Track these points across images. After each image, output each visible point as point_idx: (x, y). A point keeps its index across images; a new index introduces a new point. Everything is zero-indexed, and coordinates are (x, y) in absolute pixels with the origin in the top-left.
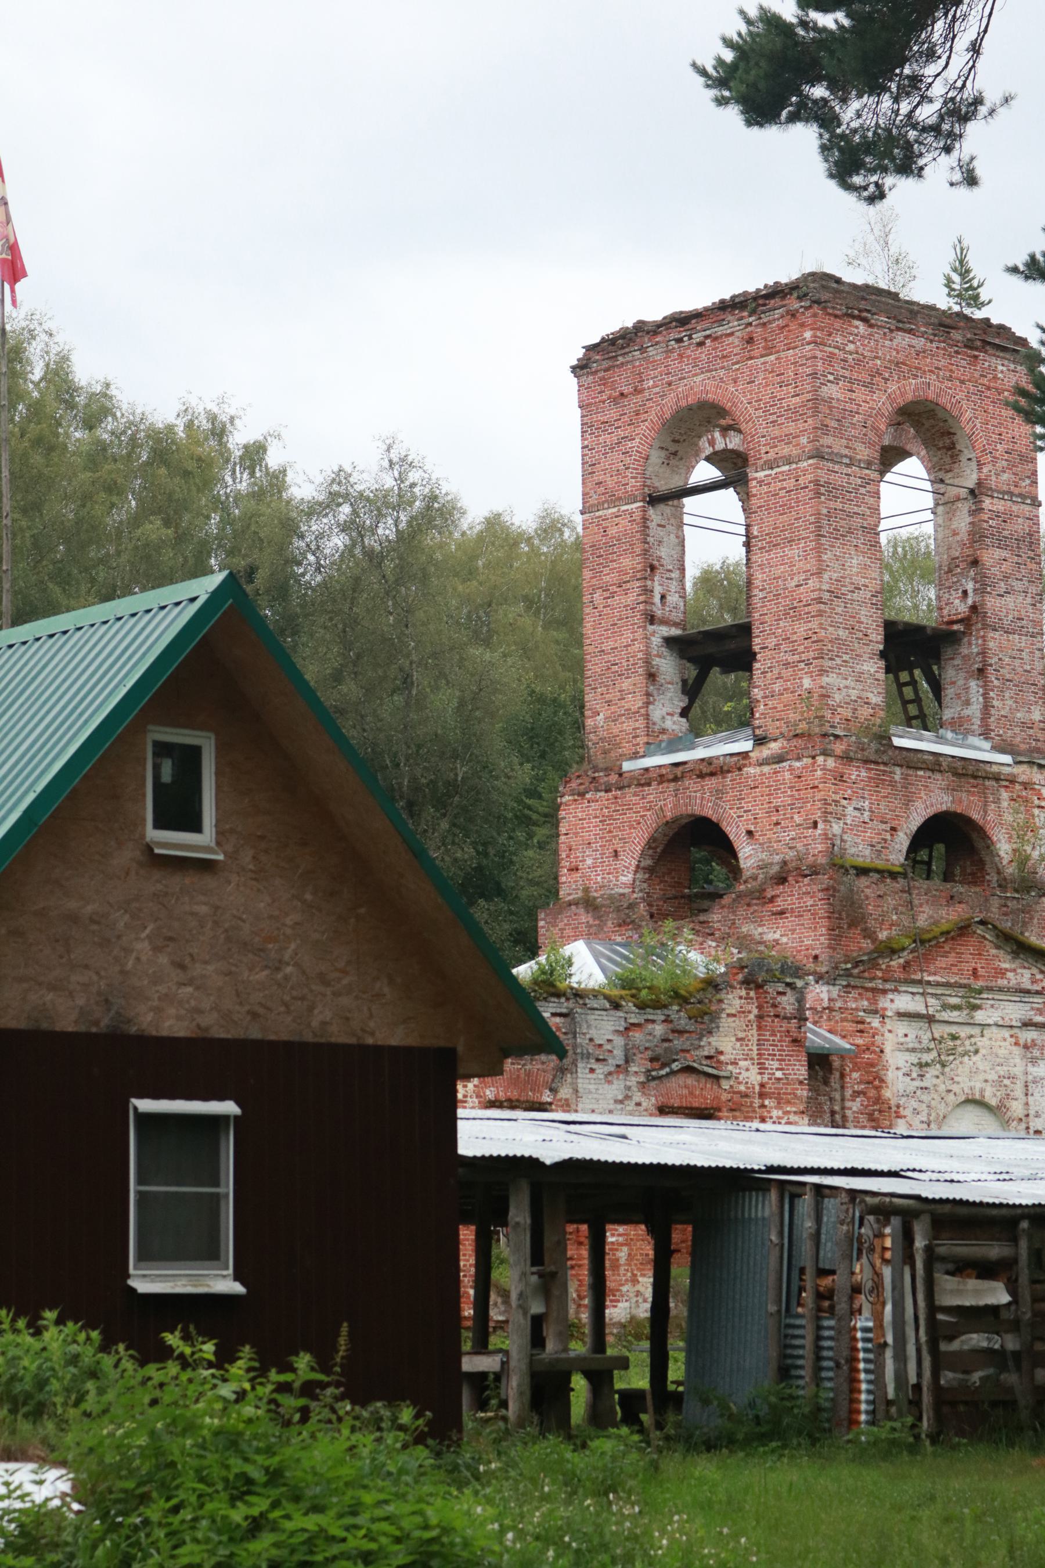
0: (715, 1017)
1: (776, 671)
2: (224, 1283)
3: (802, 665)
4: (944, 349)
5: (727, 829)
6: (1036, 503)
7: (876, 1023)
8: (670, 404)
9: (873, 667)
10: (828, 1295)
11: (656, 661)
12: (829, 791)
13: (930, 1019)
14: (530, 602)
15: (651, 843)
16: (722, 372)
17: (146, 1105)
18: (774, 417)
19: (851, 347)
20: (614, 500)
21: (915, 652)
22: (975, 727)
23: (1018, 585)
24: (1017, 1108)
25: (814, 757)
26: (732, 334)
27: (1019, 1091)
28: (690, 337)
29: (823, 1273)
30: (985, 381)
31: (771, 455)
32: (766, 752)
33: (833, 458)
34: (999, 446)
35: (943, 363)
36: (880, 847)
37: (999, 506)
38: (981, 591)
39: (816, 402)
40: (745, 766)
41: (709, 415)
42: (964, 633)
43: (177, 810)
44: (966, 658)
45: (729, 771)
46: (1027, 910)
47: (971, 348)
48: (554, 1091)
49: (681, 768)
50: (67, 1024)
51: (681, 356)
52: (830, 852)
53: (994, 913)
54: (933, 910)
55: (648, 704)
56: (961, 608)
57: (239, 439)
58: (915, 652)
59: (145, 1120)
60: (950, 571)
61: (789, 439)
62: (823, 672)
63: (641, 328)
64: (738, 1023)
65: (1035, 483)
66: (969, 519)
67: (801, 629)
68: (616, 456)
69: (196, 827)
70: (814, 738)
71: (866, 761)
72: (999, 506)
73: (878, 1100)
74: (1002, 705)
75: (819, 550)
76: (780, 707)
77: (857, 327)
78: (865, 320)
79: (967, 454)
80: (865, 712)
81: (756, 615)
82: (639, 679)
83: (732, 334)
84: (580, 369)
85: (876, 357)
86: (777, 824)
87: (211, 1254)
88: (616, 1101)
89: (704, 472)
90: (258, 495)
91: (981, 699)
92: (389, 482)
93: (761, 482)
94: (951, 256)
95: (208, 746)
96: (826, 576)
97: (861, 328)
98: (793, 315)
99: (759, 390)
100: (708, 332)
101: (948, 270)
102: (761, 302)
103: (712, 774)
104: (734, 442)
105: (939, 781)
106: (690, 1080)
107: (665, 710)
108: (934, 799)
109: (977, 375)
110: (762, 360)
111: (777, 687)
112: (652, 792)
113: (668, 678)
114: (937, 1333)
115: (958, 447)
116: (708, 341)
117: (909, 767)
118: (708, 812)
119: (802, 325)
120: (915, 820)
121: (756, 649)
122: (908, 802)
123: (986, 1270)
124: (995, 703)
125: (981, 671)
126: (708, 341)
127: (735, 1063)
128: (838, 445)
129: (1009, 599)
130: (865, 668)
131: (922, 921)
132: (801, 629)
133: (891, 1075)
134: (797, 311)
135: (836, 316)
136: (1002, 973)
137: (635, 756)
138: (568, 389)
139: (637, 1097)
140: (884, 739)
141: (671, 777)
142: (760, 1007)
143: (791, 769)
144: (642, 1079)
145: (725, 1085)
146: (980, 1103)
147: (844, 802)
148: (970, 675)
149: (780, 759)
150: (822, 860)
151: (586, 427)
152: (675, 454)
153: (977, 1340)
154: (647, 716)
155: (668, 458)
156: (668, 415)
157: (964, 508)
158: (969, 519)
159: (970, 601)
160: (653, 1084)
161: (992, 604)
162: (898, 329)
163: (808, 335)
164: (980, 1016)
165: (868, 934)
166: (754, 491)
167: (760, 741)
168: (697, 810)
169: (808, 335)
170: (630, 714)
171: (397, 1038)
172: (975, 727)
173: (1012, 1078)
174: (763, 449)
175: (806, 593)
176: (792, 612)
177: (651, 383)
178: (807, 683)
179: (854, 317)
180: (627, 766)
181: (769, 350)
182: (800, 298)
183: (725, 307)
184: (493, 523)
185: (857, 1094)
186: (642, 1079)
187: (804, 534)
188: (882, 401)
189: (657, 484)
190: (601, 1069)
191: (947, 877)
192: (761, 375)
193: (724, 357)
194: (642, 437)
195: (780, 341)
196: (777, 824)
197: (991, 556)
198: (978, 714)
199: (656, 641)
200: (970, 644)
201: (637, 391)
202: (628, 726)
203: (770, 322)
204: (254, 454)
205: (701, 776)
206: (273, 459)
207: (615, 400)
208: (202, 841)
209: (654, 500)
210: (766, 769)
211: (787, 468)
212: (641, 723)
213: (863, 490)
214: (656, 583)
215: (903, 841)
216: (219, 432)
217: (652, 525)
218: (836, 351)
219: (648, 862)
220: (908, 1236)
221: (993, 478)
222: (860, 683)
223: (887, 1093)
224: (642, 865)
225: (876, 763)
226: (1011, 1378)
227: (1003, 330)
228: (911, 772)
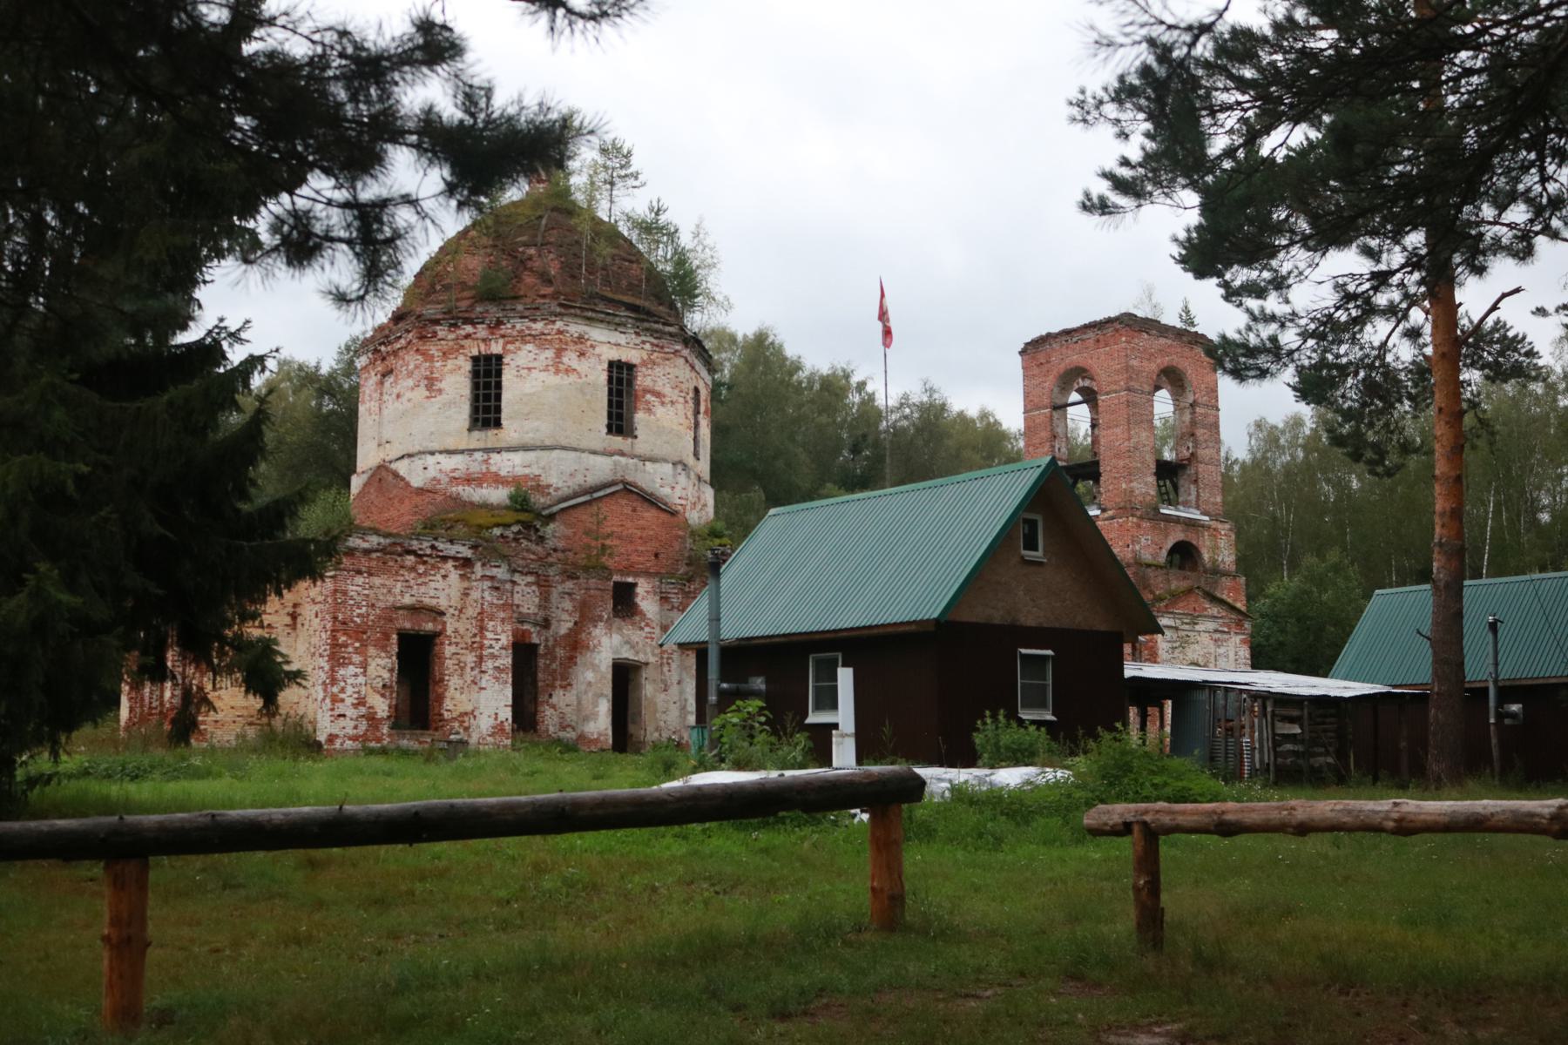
2: (1050, 717)
8: (1062, 367)
9: (1152, 479)
10: (1231, 729)
12: (1134, 532)
13: (1176, 629)
14: (974, 448)
17: (1024, 651)
20: (1039, 408)
21: (1168, 472)
29: (1228, 721)
36: (1155, 556)
38: (1195, 447)
39: (1127, 368)
41: (1080, 372)
43: (1031, 544)
50: (997, 621)
52: (1135, 558)
53: (1202, 584)
54: (1177, 584)
56: (1186, 454)
57: (854, 380)
58: (1168, 472)
59: (1023, 656)
61: (1116, 382)
63: (1049, 335)
67: (1121, 463)
69: (1036, 549)
70: (1127, 509)
74: (1205, 495)
84: (1023, 352)
87: (1042, 705)
89: (1075, 397)
90: (863, 403)
92: (925, 399)
94: (1181, 305)
95: (1039, 519)
99: (1103, 363)
104: (1087, 383)
105: (1179, 527)
108: (1177, 535)
114: (1276, 744)
120: (1170, 544)
122: (1166, 537)
123: (1292, 720)
125: (1196, 481)
131: (1173, 587)
132: (1121, 463)
140: (1156, 509)
149: (1112, 518)
151: (1025, 376)
153: (1289, 747)
157: (1188, 412)
161: (1201, 453)
164: (1197, 627)
165: (1152, 592)
167: (1104, 510)
171: (1103, 628)
176: (1118, 456)
183: (1087, 327)
184: (961, 414)
188: (1153, 367)
191: (1181, 568)
194: (1050, 382)
197: (1200, 432)
204: (861, 386)
206: (869, 388)
208: (1038, 555)
215: (1164, 553)
216: (847, 376)
220: (1264, 707)
222: (1146, 486)
226: (1300, 762)
227: (1203, 336)
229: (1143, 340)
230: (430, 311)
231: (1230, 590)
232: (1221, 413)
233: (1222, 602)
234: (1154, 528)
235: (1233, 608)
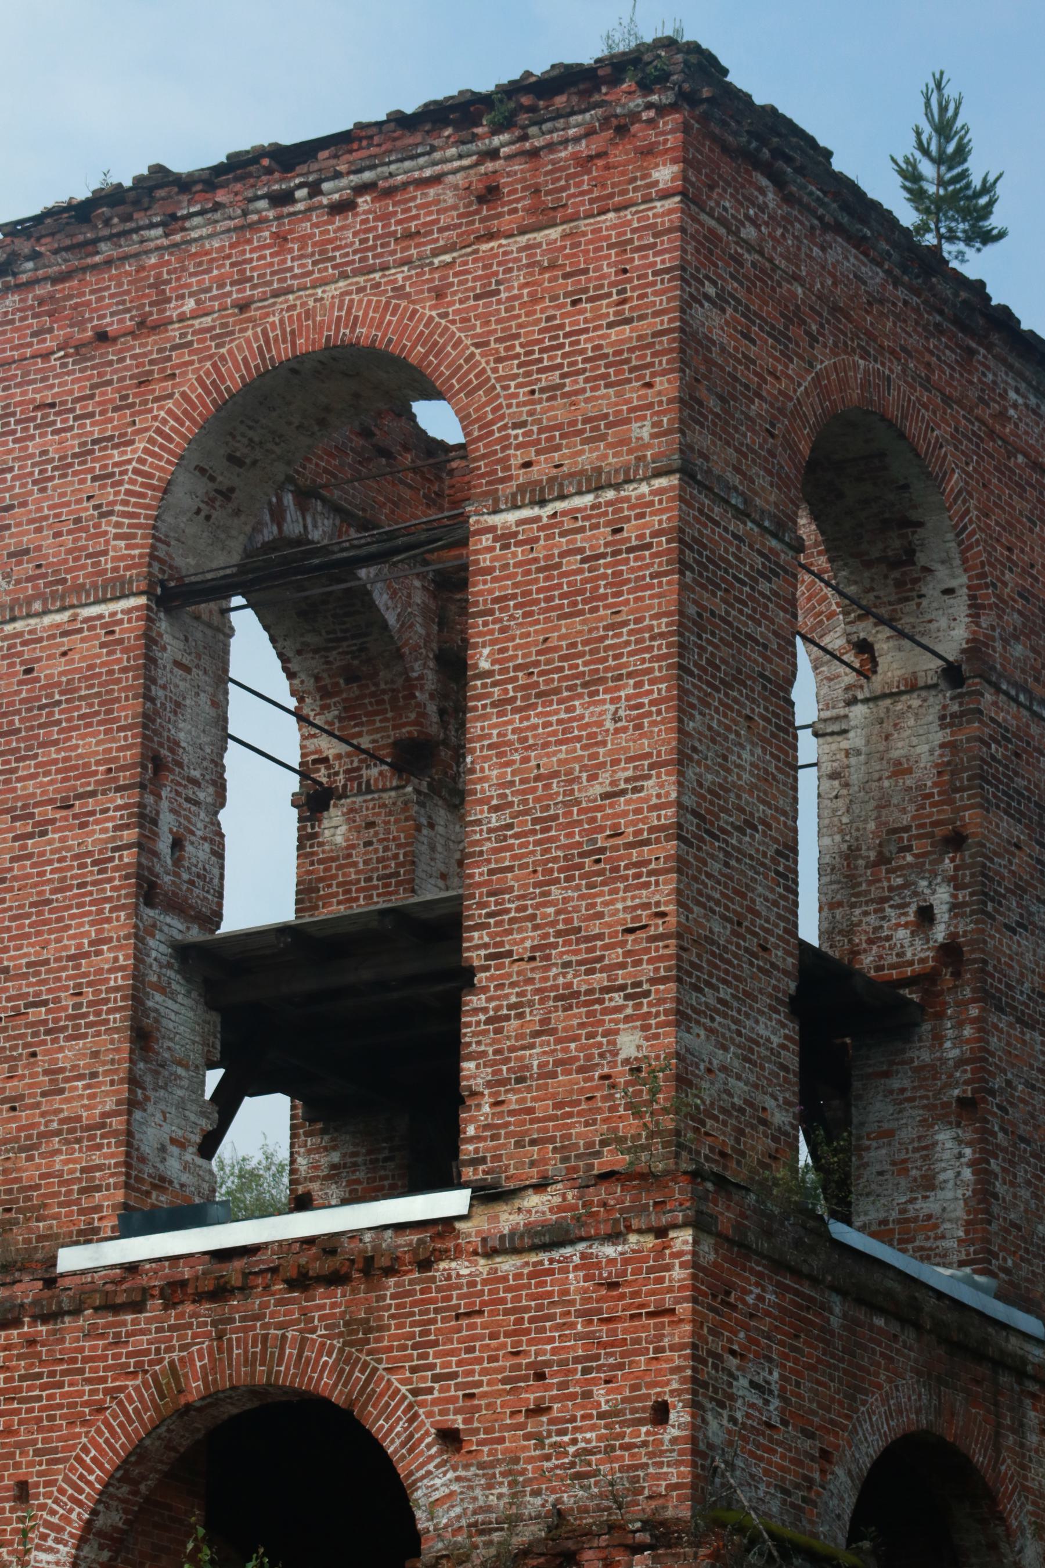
1: (533, 1017)
3: (618, 998)
4: (916, 310)
5: (379, 1426)
11: (156, 1000)
15: (127, 1472)
16: (400, 275)
18: (555, 377)
22: (950, 1244)
25: (661, 1232)
26: (436, 180)
28: (315, 190)
30: (986, 414)
31: (542, 470)
32: (507, 1219)
34: (1008, 576)
35: (914, 341)
40: (443, 1255)
42: (921, 1007)
44: (927, 1073)
45: (390, 1271)
47: (964, 328)
49: (238, 1264)
51: (281, 239)
55: (132, 1104)
60: (882, 860)
61: (596, 428)
63: (158, 182)
66: (939, 737)
68: (72, 487)
71: (779, 1265)
76: (544, 1108)
77: (762, 191)
78: (779, 182)
81: (479, 873)
82: (113, 1043)
83: (436, 180)
85: (796, 278)
86: (539, 1410)
91: (967, 1174)
93: (505, 538)
98: (622, 130)
100: (367, 176)
101: (907, 148)
102: (526, 100)
103: (336, 1279)
107: (171, 1129)
109: (973, 394)
110: (523, 240)
111: (534, 1058)
112: (144, 1329)
113: (179, 1052)
115: (921, 559)
116: (364, 202)
117: (860, 1301)
118: (325, 1383)
119: (648, 152)
120: (868, 1444)
121: (475, 957)
124: (1000, 1188)
126: (364, 202)
129: (1024, 941)
130: (761, 1029)
134: (634, 116)
135: (725, 149)
137: (88, 1236)
141: (208, 1285)
143: (588, 1263)
147: (733, 1362)
148: (942, 1113)
149: (551, 1237)
150: (678, 1509)
152: (226, 494)
155: (210, 502)
156: (234, 382)
158: (939, 737)
159: (939, 934)
162: (838, 229)
166: (485, 560)
167: (487, 1195)
168: (287, 1374)
172: (950, 1244)
174: (517, 457)
177: (190, 304)
179: (758, 164)
180: (71, 1259)
181: (544, 216)
182: (645, 87)
187: (633, 663)
189: (179, 562)
192: (519, 277)
193: (409, 236)
195: (578, 193)
196: (539, 1410)
198: (959, 1211)
199: (158, 949)
200: (938, 1038)
201: (145, 327)
202: (68, 1161)
203: (551, 147)
205: (302, 1282)
207: (79, 350)
210: (508, 1265)
211: (588, 499)
213: (764, 586)
214: (165, 805)
217: (165, 658)
218: (722, 231)
219: (113, 1519)
221: (999, 645)
224: (99, 1523)
225: (796, 1273)
228: (861, 1314)
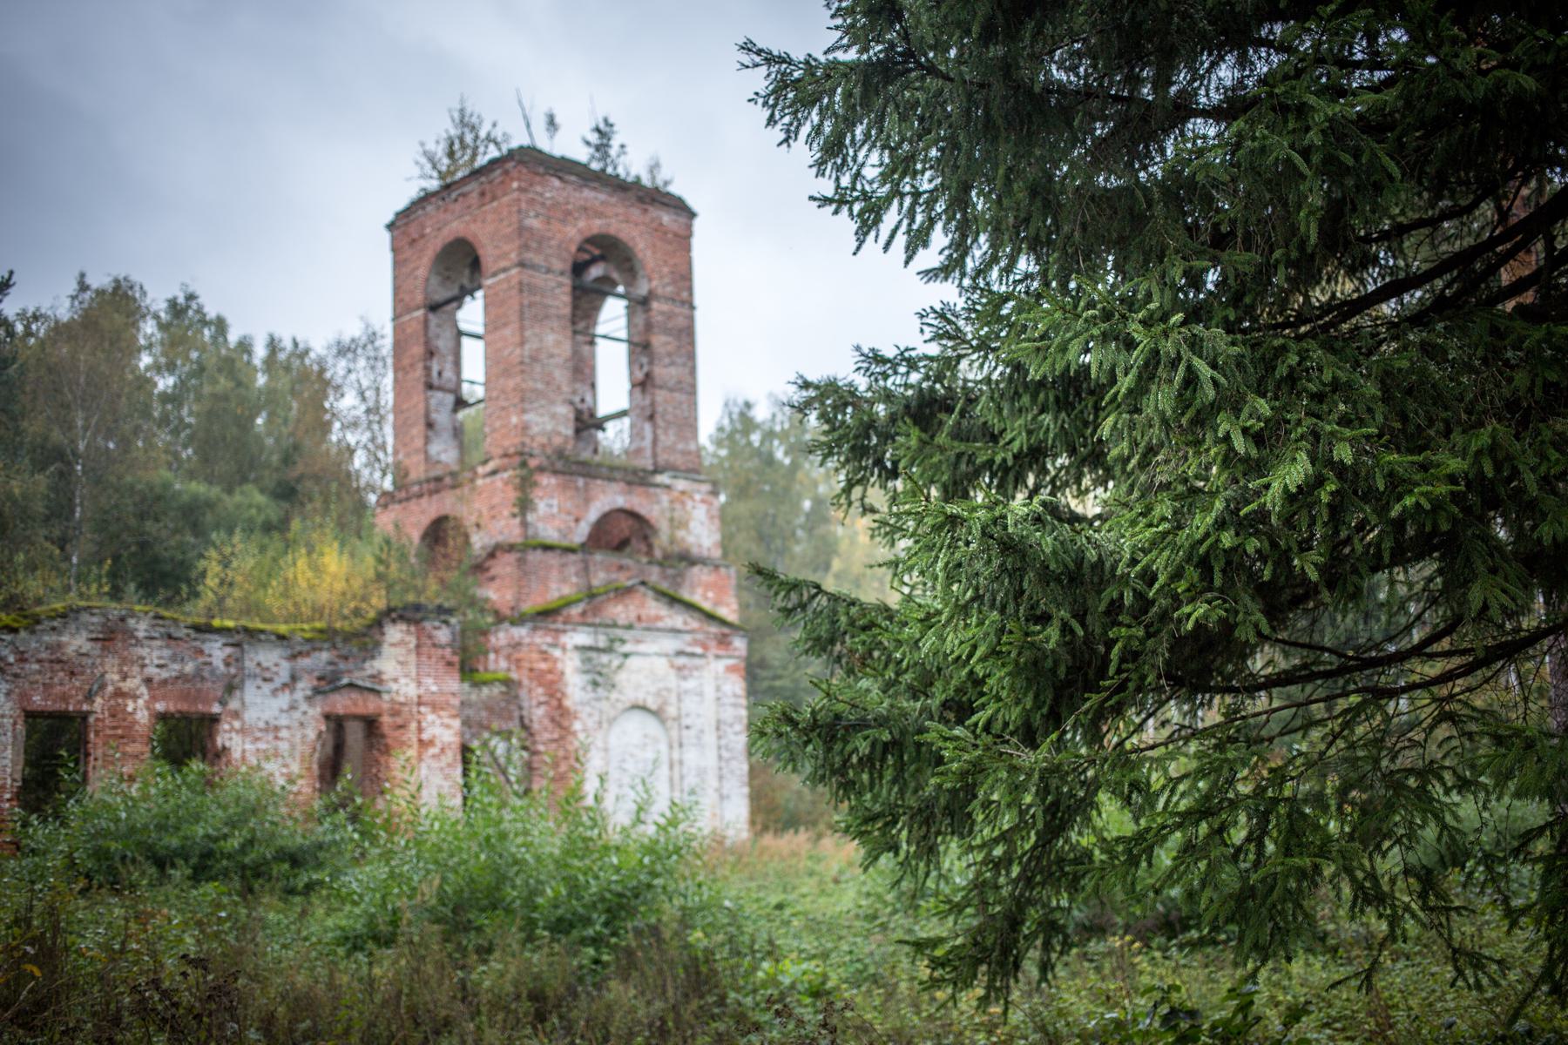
0: (378, 645)
6: (692, 308)
7: (557, 653)
19: (548, 195)
20: (409, 310)
23: (679, 361)
24: (671, 711)
27: (673, 699)
33: (533, 267)
37: (665, 307)
39: (521, 230)
46: (681, 575)
48: (223, 703)
61: (505, 255)
62: (524, 411)
64: (401, 651)
65: (691, 294)
67: (511, 383)
71: (555, 472)
72: (665, 307)
73: (560, 706)
75: (522, 328)
79: (641, 273)
80: (557, 441)
84: (391, 227)
88: (282, 711)
96: (527, 347)
97: (556, 183)
106: (355, 695)
122: (587, 501)
127: (395, 680)
128: (538, 259)
129: (673, 371)
132: (511, 383)
133: (570, 690)
136: (658, 618)
138: (386, 237)
139: (304, 707)
142: (418, 638)
144: (309, 693)
145: (386, 697)
146: (643, 708)
149: (494, 473)
154: (426, 452)
160: (319, 697)
163: (515, 185)
169: (515, 185)
170: (417, 451)
173: (668, 690)
175: (515, 359)
178: (514, 420)
181: (494, 198)
185: (540, 704)
186: (309, 693)
190: (267, 688)
209: (434, 308)
212: (422, 456)
223: (567, 703)
229: (553, 189)
230: (494, 394)
231: (708, 587)
232: (699, 316)
233: (690, 607)
234: (564, 487)
235: (711, 617)
